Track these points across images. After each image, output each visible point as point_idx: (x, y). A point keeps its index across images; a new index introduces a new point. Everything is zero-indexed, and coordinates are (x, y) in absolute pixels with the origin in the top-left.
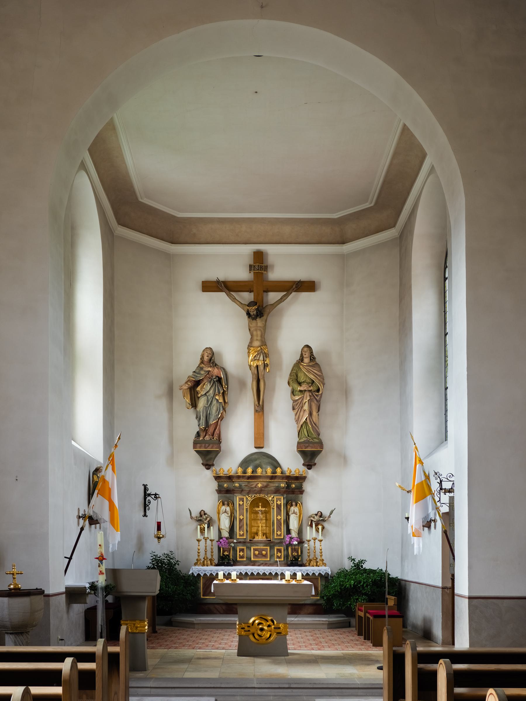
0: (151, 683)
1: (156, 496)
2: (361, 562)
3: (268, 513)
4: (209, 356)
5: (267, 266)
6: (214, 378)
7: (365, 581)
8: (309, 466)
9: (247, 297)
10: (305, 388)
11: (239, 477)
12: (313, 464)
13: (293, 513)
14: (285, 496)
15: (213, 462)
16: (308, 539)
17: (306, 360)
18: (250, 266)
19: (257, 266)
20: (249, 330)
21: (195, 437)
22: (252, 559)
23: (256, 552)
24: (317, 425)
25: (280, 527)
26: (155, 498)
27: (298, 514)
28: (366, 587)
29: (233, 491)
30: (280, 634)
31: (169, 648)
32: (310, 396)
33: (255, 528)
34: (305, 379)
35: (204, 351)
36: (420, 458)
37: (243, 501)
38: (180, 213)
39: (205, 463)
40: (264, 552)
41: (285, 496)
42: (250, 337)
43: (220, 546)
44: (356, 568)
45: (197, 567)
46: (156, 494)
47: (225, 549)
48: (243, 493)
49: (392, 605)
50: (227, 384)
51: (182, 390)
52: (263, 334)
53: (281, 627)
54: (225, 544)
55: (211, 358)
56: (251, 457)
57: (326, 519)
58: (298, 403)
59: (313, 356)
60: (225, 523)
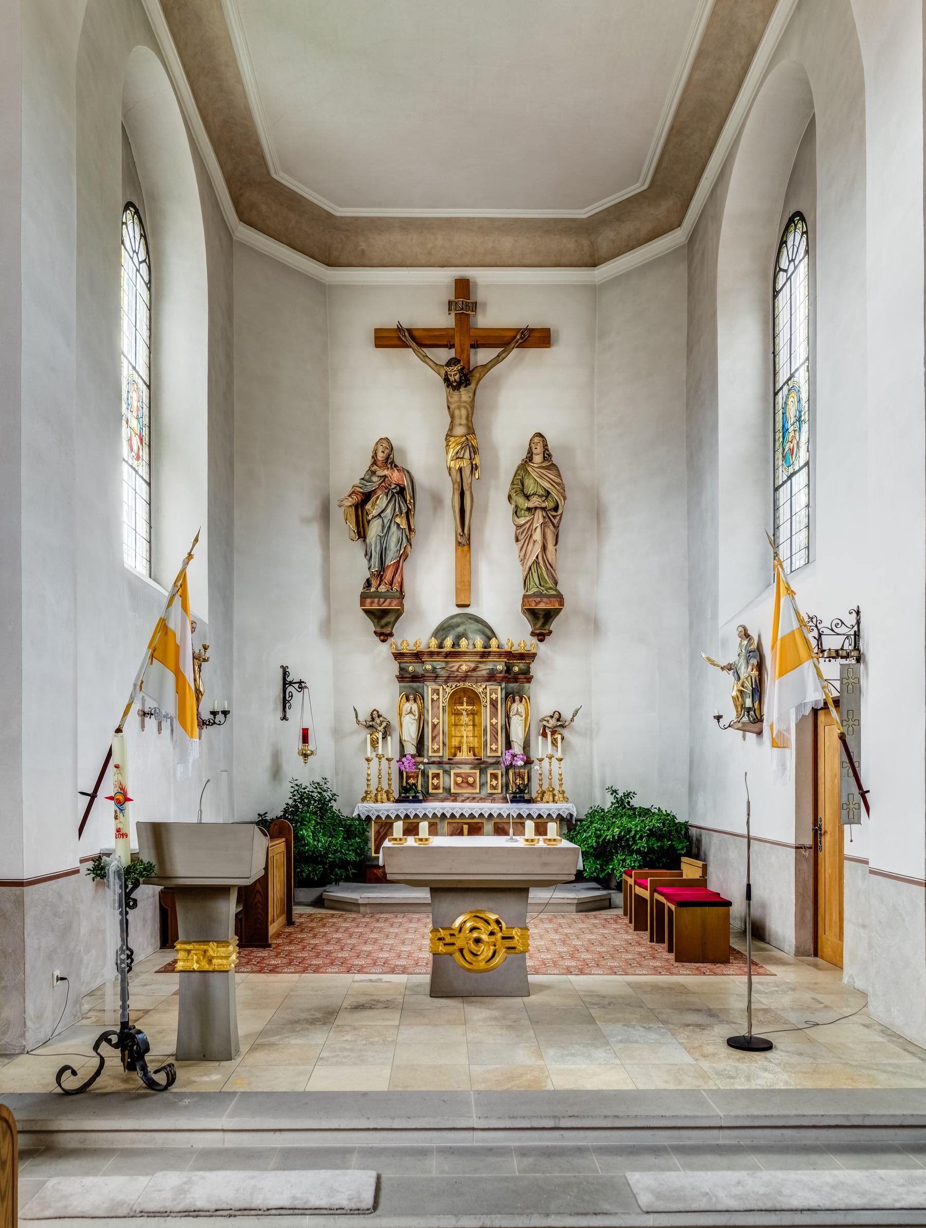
0: (224, 1119)
1: (301, 685)
2: (628, 795)
3: (476, 714)
4: (385, 452)
5: (476, 303)
6: (392, 487)
7: (638, 829)
8: (541, 637)
9: (443, 355)
10: (537, 504)
11: (431, 654)
12: (547, 631)
13: (516, 714)
14: (503, 685)
15: (392, 628)
16: (540, 757)
17: (538, 459)
18: (450, 303)
19: (461, 303)
20: (449, 408)
21: (364, 588)
22: (453, 791)
23: (458, 779)
24: (553, 567)
25: (495, 737)
26: (299, 688)
27: (524, 716)
28: (638, 839)
29: (422, 677)
30: (513, 951)
31: (304, 972)
32: (544, 517)
33: (458, 738)
34: (535, 490)
35: (377, 444)
36: (787, 584)
37: (438, 694)
38: (341, 209)
39: (379, 630)
40: (471, 780)
41: (503, 685)
42: (449, 420)
43: (403, 768)
44: (618, 807)
45: (365, 804)
46: (301, 682)
47: (410, 774)
48: (439, 680)
49: (699, 878)
50: (413, 498)
51: (343, 509)
52: (470, 416)
53: (515, 936)
54: (409, 766)
55: (389, 455)
56: (450, 622)
57: (566, 724)
58: (525, 529)
59: (547, 452)
60: (410, 731)
